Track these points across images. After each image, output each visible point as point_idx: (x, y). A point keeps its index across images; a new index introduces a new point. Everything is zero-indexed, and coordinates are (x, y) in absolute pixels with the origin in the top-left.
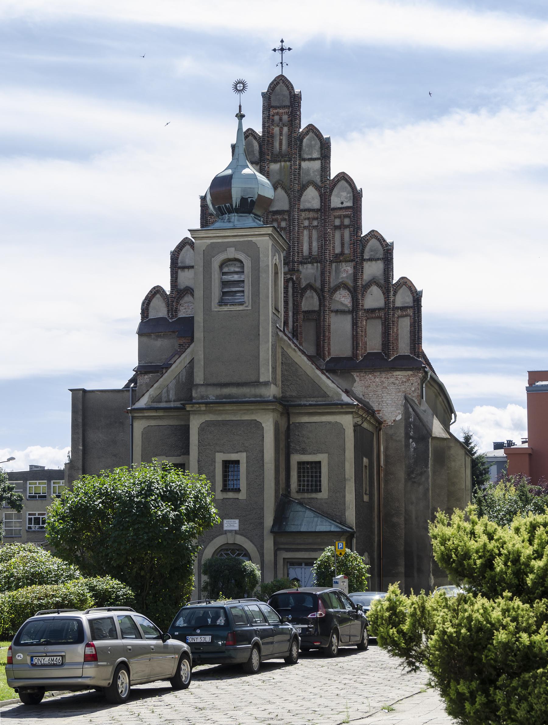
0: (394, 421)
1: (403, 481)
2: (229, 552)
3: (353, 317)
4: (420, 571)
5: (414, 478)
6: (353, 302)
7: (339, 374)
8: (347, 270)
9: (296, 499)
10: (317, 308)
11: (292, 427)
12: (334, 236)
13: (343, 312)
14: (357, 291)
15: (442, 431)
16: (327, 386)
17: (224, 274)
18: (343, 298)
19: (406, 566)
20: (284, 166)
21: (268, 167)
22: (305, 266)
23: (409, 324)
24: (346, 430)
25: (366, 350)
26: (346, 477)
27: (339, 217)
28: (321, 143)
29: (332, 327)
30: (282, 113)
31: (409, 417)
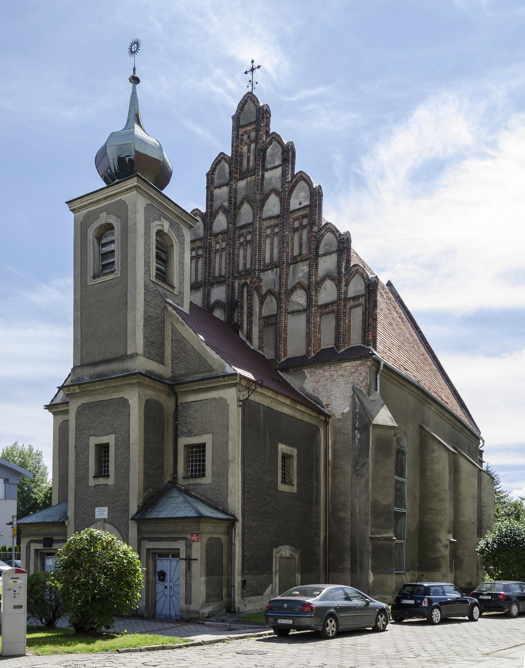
0: (342, 414)
1: (350, 474)
4: (361, 566)
7: (291, 372)
9: (182, 486)
11: (179, 408)
12: (293, 239)
13: (298, 312)
15: (389, 420)
16: (213, 359)
17: (104, 245)
18: (299, 298)
20: (250, 180)
22: (266, 273)
23: (361, 313)
24: (230, 405)
25: (320, 347)
26: (230, 458)
27: (297, 219)
28: (282, 148)
29: (288, 328)
30: (250, 130)
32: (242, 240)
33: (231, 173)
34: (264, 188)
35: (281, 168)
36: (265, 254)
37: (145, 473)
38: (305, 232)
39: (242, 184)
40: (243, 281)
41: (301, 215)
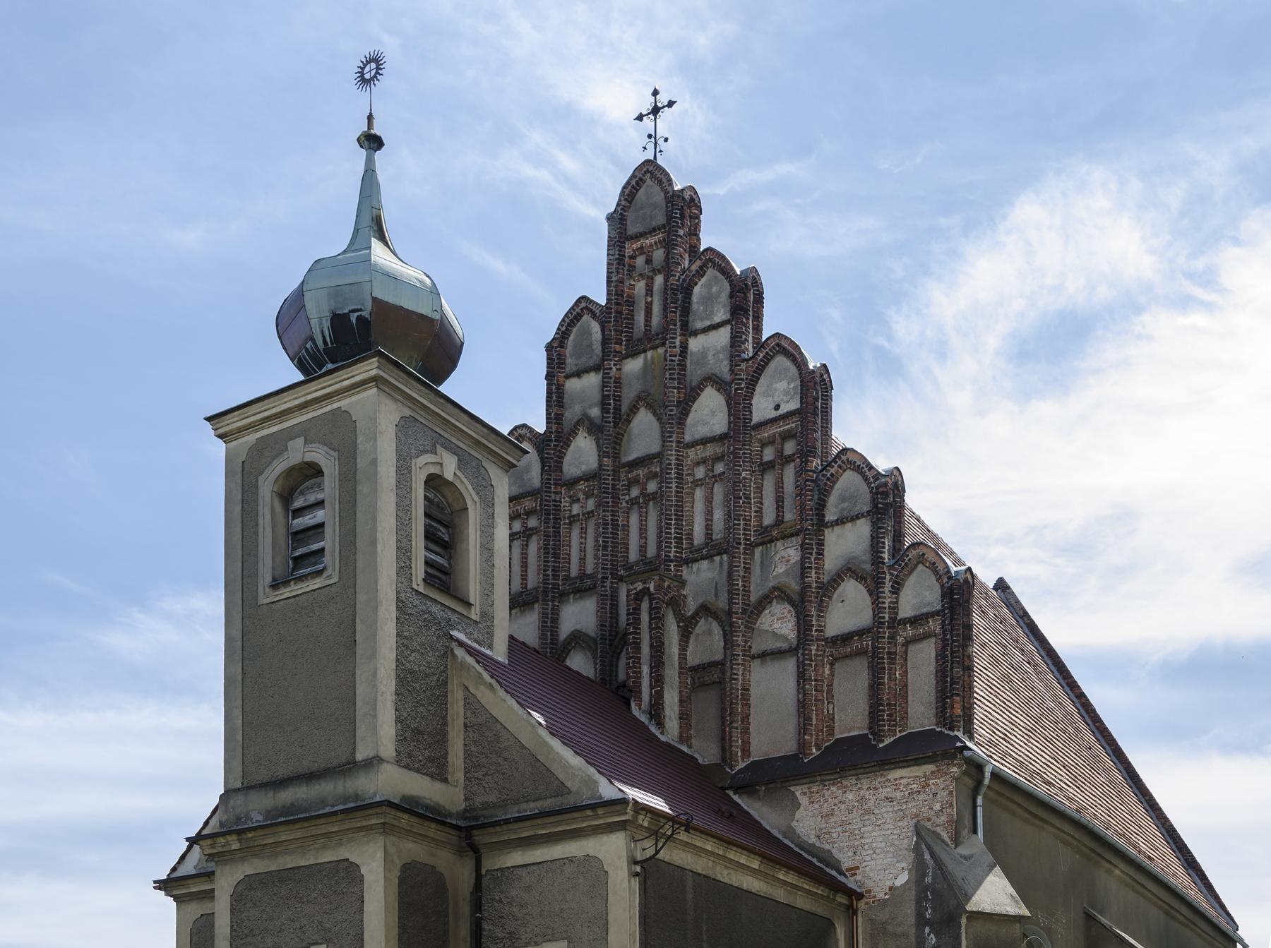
0: (891, 888)
7: (762, 793)
8: (788, 554)
10: (719, 657)
11: (485, 881)
12: (760, 488)
13: (777, 654)
16: (566, 767)
18: (779, 623)
20: (652, 358)
21: (620, 369)
22: (695, 566)
23: (933, 654)
24: (610, 873)
25: (831, 732)
27: (771, 442)
28: (731, 282)
29: (753, 691)
31: (924, 875)
32: (635, 492)
34: (688, 373)
36: (691, 524)
39: (633, 366)
40: (639, 586)
41: (780, 434)
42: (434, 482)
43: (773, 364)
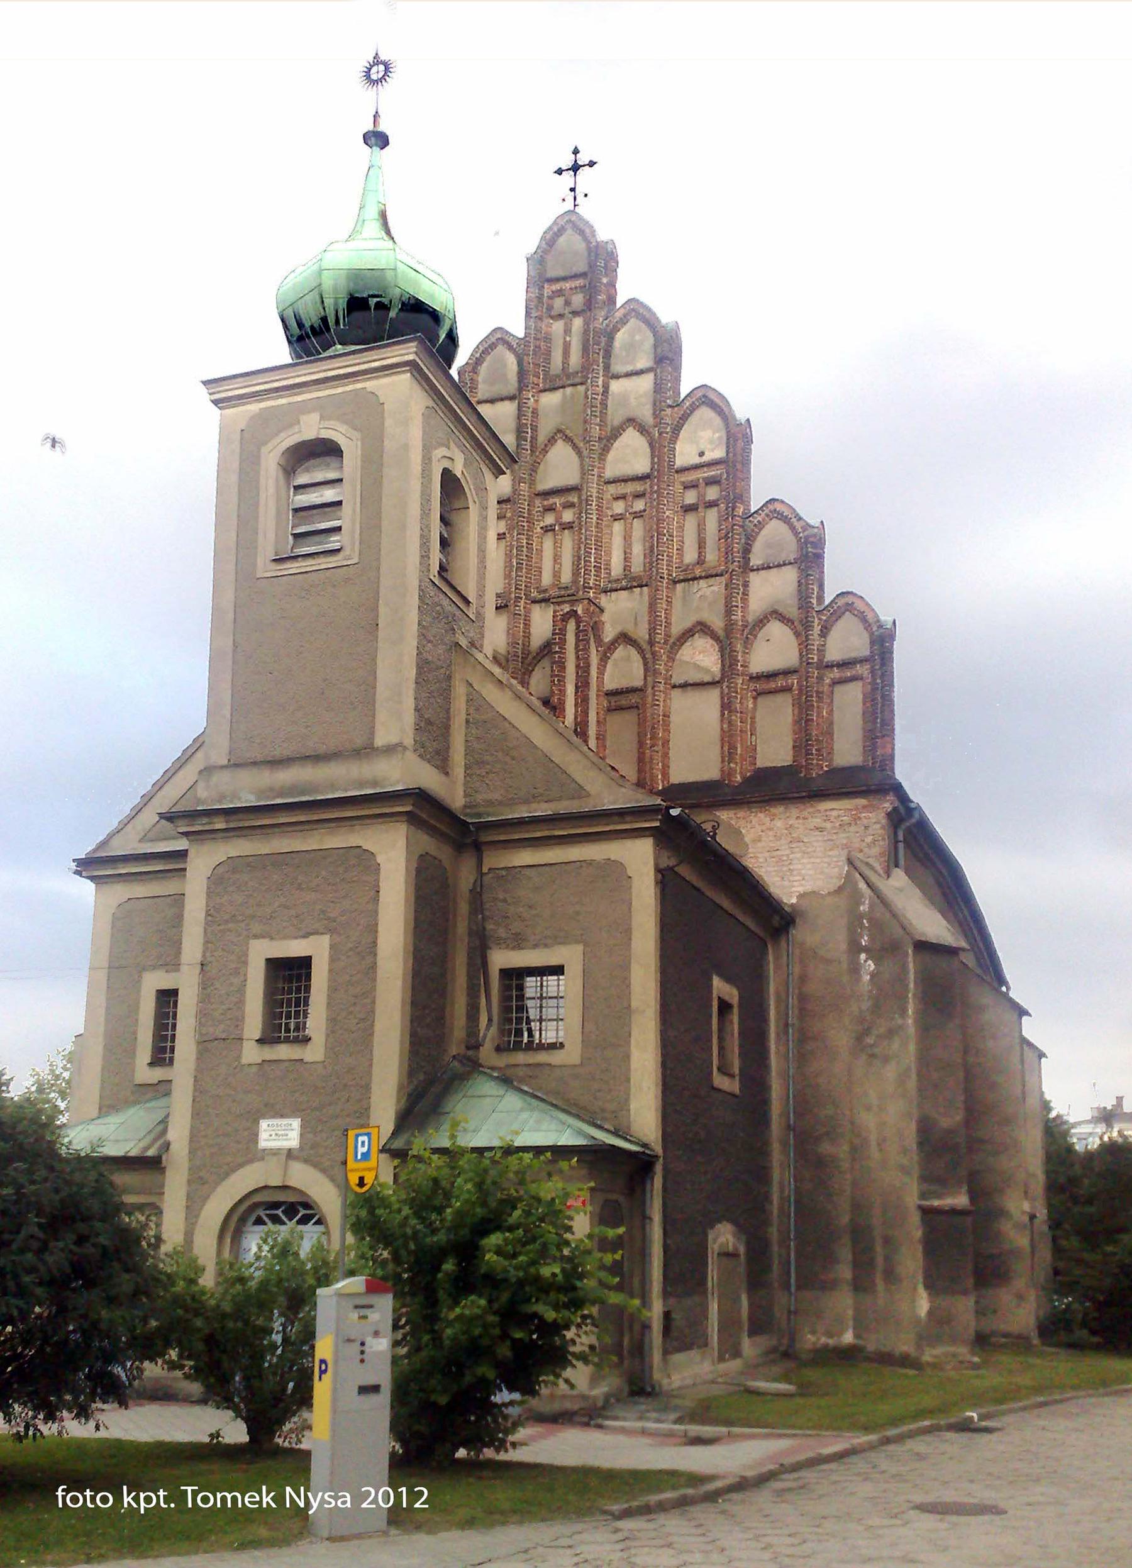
2: (279, 1212)
3: (722, 693)
4: (890, 1275)
5: (872, 1046)
6: (723, 665)
10: (639, 683)
12: (681, 528)
14: (731, 639)
18: (703, 657)
19: (856, 1265)
20: (573, 395)
21: (536, 401)
29: (673, 718)
31: (858, 903)
33: (522, 374)
34: (609, 413)
35: (651, 376)
36: (609, 554)
37: (413, 1034)
38: (712, 517)
39: (551, 400)
40: (566, 608)
41: (704, 479)
42: (447, 474)
43: (697, 414)
